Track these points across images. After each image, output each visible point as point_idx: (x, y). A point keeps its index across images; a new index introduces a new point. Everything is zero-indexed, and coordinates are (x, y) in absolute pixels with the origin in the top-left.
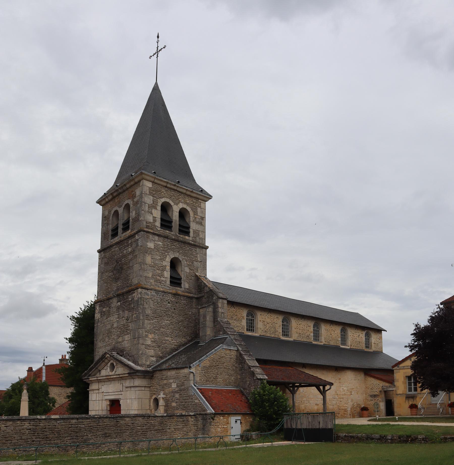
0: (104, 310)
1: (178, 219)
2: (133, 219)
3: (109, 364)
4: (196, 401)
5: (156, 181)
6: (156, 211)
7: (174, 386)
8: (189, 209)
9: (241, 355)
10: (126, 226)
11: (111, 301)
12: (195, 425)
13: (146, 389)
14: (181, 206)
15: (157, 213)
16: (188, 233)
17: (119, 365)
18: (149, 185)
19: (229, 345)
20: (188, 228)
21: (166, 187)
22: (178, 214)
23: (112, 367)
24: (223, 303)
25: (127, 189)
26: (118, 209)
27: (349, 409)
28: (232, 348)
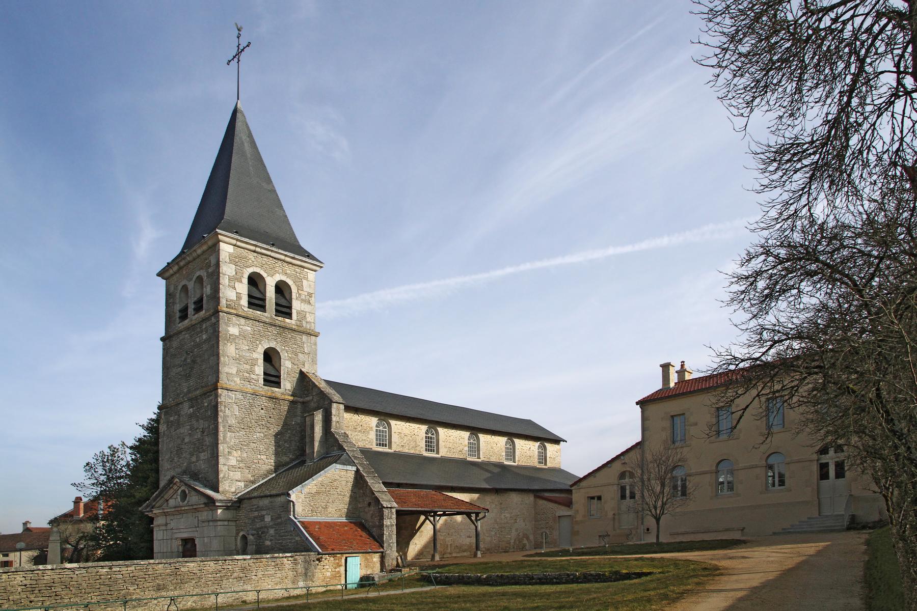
0: (172, 419)
1: (274, 297)
2: (207, 296)
3: (180, 491)
4: (297, 538)
5: (239, 244)
6: (240, 284)
7: (268, 519)
8: (290, 282)
9: (362, 477)
10: (199, 306)
11: (181, 406)
12: (294, 569)
13: (230, 523)
14: (278, 277)
15: (243, 288)
16: (289, 315)
17: (193, 493)
18: (230, 249)
19: (344, 464)
20: (290, 308)
21: (254, 252)
22: (273, 289)
23: (184, 496)
24: (338, 409)
25: (199, 256)
26: (187, 283)
27: (512, 541)
28: (349, 468)
